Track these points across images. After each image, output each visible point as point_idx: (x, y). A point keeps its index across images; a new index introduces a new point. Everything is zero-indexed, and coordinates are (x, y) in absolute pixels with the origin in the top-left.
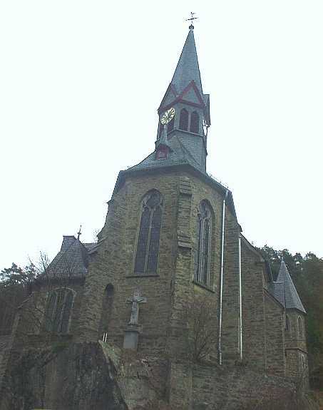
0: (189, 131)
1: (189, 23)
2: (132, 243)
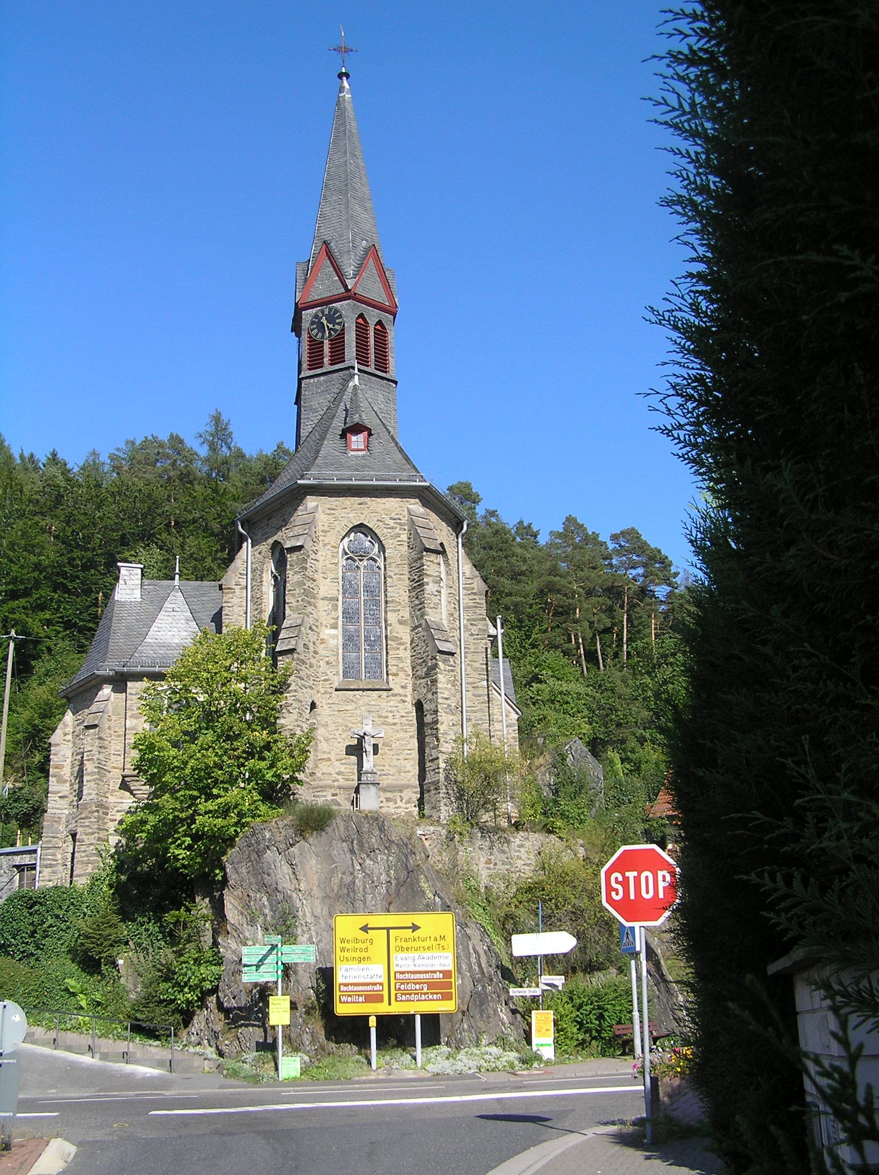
2: (334, 626)
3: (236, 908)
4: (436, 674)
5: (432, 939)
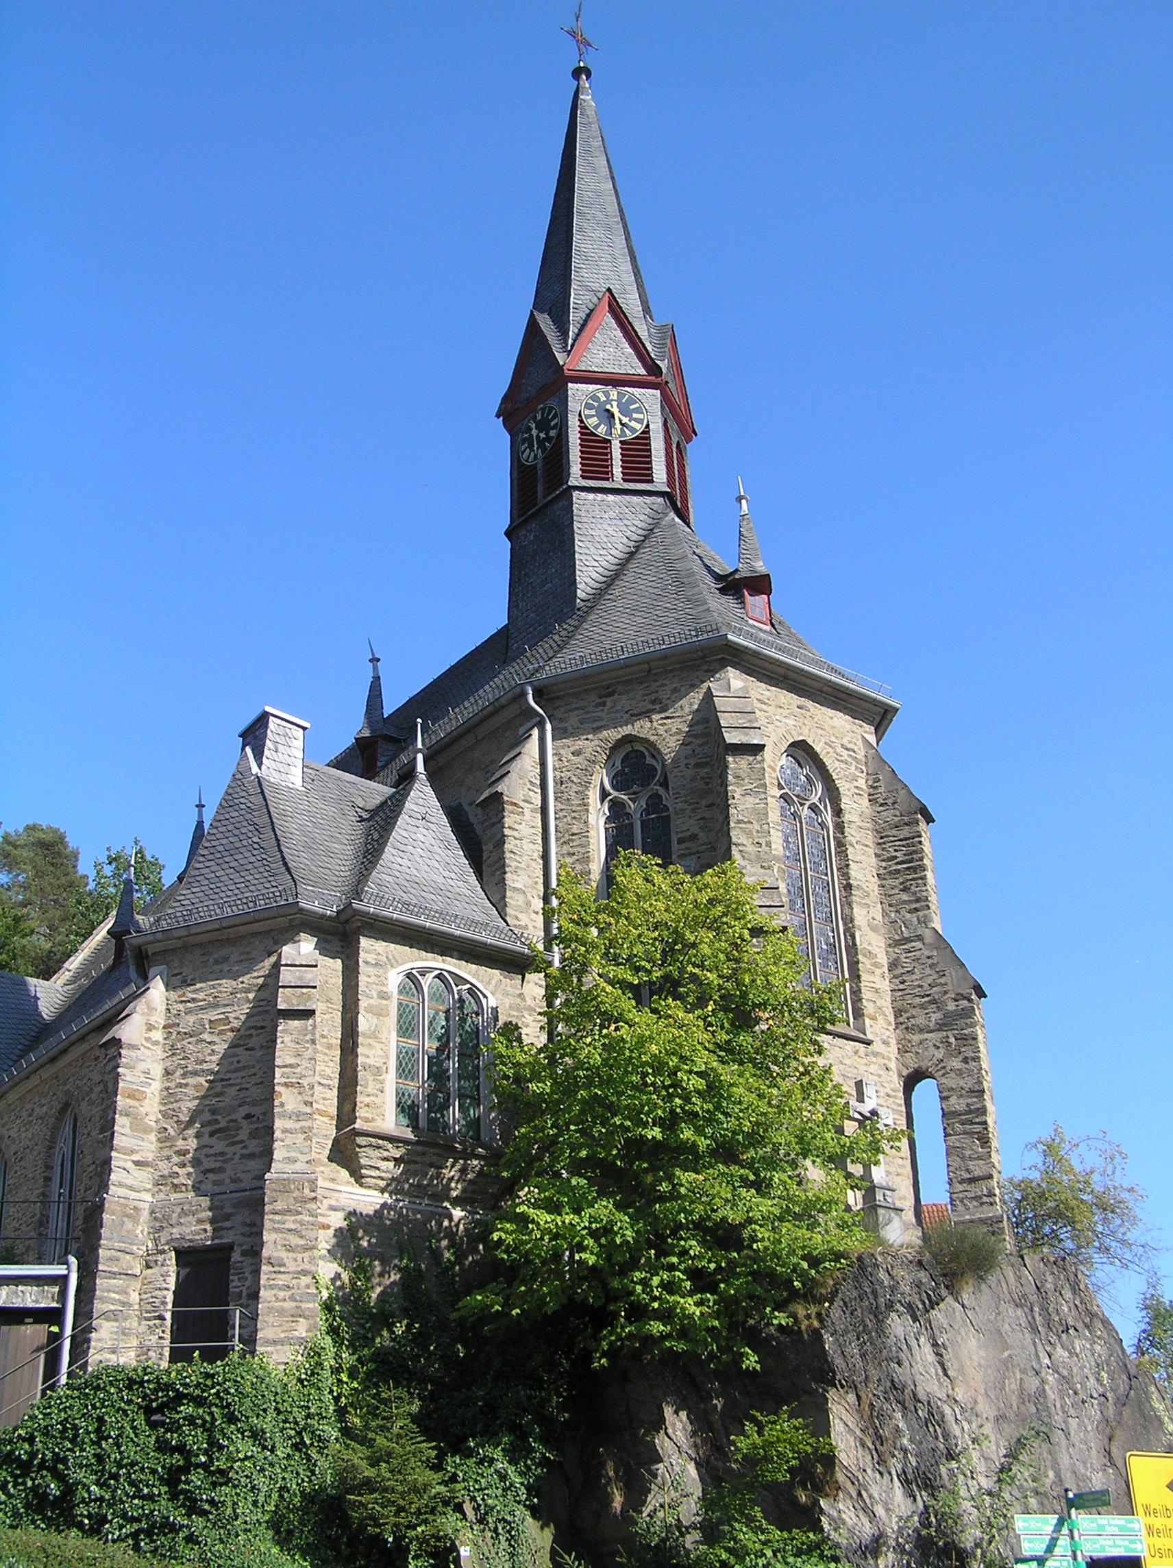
3: (850, 1430)
4: (973, 1025)
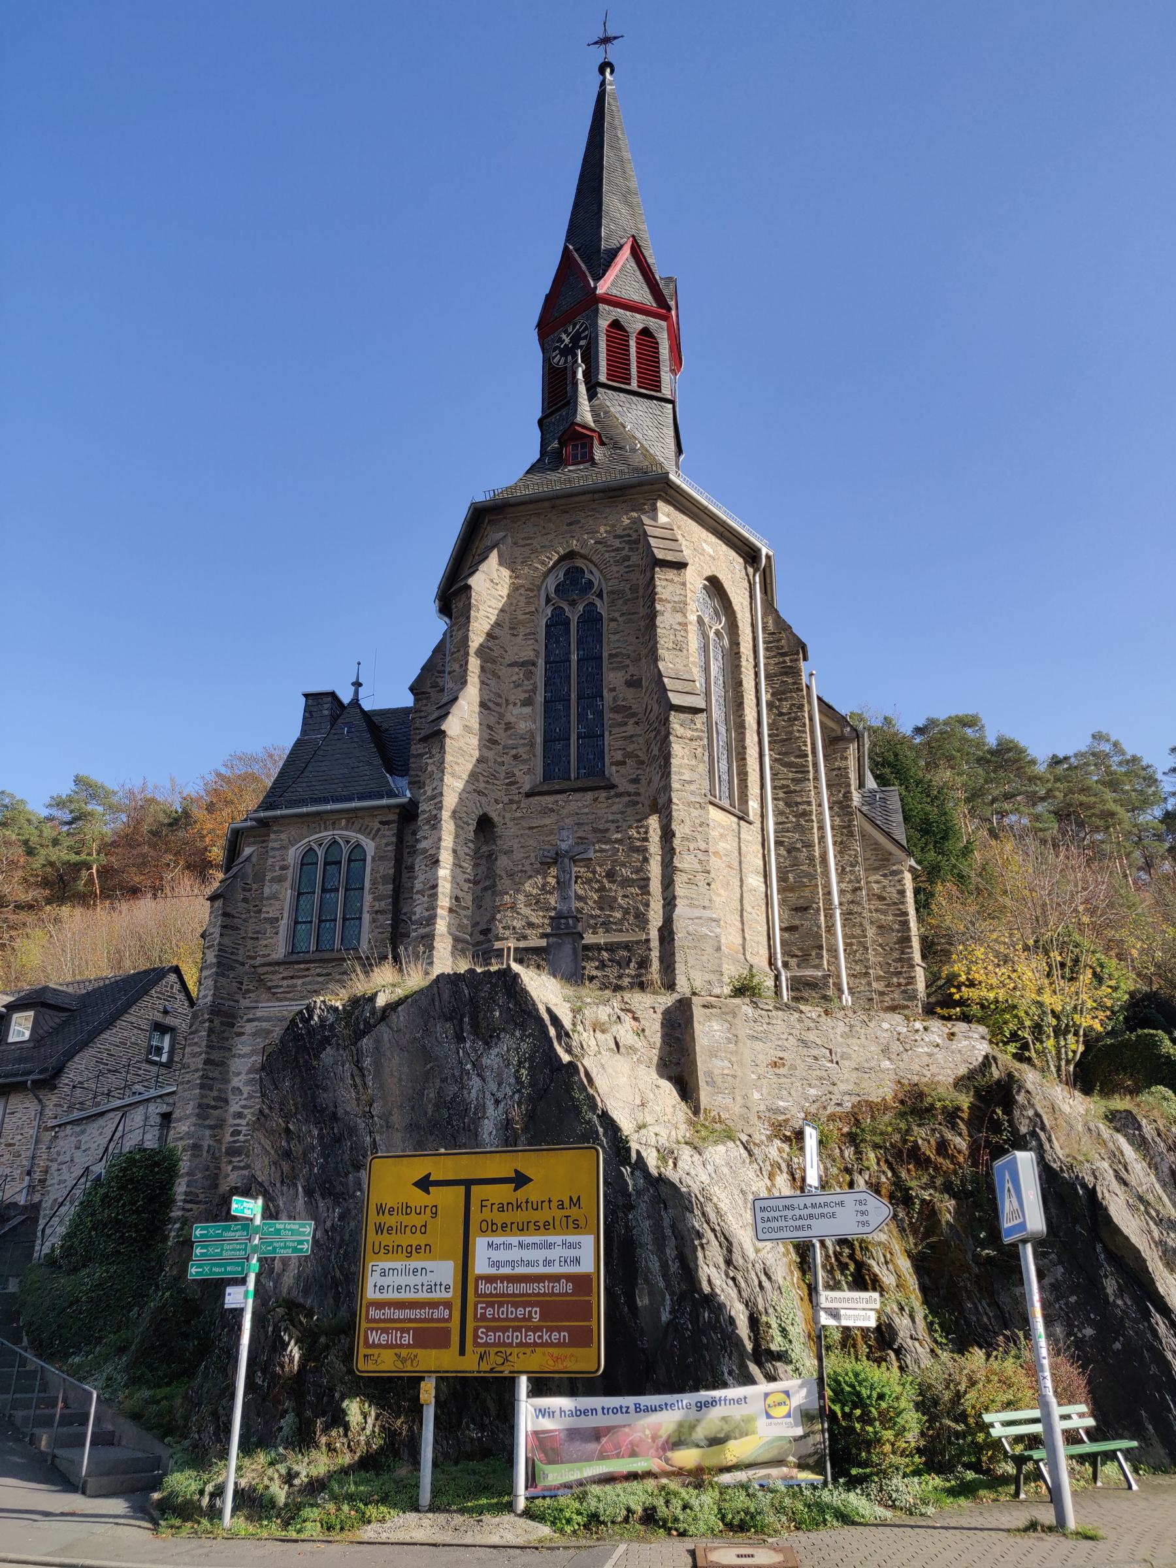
0: (634, 385)
1: (598, 55)
2: (528, 702)
5: (554, 1204)
